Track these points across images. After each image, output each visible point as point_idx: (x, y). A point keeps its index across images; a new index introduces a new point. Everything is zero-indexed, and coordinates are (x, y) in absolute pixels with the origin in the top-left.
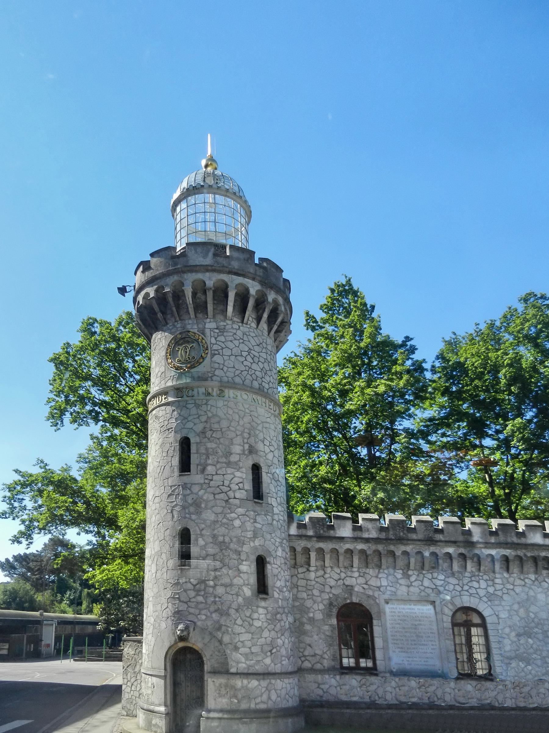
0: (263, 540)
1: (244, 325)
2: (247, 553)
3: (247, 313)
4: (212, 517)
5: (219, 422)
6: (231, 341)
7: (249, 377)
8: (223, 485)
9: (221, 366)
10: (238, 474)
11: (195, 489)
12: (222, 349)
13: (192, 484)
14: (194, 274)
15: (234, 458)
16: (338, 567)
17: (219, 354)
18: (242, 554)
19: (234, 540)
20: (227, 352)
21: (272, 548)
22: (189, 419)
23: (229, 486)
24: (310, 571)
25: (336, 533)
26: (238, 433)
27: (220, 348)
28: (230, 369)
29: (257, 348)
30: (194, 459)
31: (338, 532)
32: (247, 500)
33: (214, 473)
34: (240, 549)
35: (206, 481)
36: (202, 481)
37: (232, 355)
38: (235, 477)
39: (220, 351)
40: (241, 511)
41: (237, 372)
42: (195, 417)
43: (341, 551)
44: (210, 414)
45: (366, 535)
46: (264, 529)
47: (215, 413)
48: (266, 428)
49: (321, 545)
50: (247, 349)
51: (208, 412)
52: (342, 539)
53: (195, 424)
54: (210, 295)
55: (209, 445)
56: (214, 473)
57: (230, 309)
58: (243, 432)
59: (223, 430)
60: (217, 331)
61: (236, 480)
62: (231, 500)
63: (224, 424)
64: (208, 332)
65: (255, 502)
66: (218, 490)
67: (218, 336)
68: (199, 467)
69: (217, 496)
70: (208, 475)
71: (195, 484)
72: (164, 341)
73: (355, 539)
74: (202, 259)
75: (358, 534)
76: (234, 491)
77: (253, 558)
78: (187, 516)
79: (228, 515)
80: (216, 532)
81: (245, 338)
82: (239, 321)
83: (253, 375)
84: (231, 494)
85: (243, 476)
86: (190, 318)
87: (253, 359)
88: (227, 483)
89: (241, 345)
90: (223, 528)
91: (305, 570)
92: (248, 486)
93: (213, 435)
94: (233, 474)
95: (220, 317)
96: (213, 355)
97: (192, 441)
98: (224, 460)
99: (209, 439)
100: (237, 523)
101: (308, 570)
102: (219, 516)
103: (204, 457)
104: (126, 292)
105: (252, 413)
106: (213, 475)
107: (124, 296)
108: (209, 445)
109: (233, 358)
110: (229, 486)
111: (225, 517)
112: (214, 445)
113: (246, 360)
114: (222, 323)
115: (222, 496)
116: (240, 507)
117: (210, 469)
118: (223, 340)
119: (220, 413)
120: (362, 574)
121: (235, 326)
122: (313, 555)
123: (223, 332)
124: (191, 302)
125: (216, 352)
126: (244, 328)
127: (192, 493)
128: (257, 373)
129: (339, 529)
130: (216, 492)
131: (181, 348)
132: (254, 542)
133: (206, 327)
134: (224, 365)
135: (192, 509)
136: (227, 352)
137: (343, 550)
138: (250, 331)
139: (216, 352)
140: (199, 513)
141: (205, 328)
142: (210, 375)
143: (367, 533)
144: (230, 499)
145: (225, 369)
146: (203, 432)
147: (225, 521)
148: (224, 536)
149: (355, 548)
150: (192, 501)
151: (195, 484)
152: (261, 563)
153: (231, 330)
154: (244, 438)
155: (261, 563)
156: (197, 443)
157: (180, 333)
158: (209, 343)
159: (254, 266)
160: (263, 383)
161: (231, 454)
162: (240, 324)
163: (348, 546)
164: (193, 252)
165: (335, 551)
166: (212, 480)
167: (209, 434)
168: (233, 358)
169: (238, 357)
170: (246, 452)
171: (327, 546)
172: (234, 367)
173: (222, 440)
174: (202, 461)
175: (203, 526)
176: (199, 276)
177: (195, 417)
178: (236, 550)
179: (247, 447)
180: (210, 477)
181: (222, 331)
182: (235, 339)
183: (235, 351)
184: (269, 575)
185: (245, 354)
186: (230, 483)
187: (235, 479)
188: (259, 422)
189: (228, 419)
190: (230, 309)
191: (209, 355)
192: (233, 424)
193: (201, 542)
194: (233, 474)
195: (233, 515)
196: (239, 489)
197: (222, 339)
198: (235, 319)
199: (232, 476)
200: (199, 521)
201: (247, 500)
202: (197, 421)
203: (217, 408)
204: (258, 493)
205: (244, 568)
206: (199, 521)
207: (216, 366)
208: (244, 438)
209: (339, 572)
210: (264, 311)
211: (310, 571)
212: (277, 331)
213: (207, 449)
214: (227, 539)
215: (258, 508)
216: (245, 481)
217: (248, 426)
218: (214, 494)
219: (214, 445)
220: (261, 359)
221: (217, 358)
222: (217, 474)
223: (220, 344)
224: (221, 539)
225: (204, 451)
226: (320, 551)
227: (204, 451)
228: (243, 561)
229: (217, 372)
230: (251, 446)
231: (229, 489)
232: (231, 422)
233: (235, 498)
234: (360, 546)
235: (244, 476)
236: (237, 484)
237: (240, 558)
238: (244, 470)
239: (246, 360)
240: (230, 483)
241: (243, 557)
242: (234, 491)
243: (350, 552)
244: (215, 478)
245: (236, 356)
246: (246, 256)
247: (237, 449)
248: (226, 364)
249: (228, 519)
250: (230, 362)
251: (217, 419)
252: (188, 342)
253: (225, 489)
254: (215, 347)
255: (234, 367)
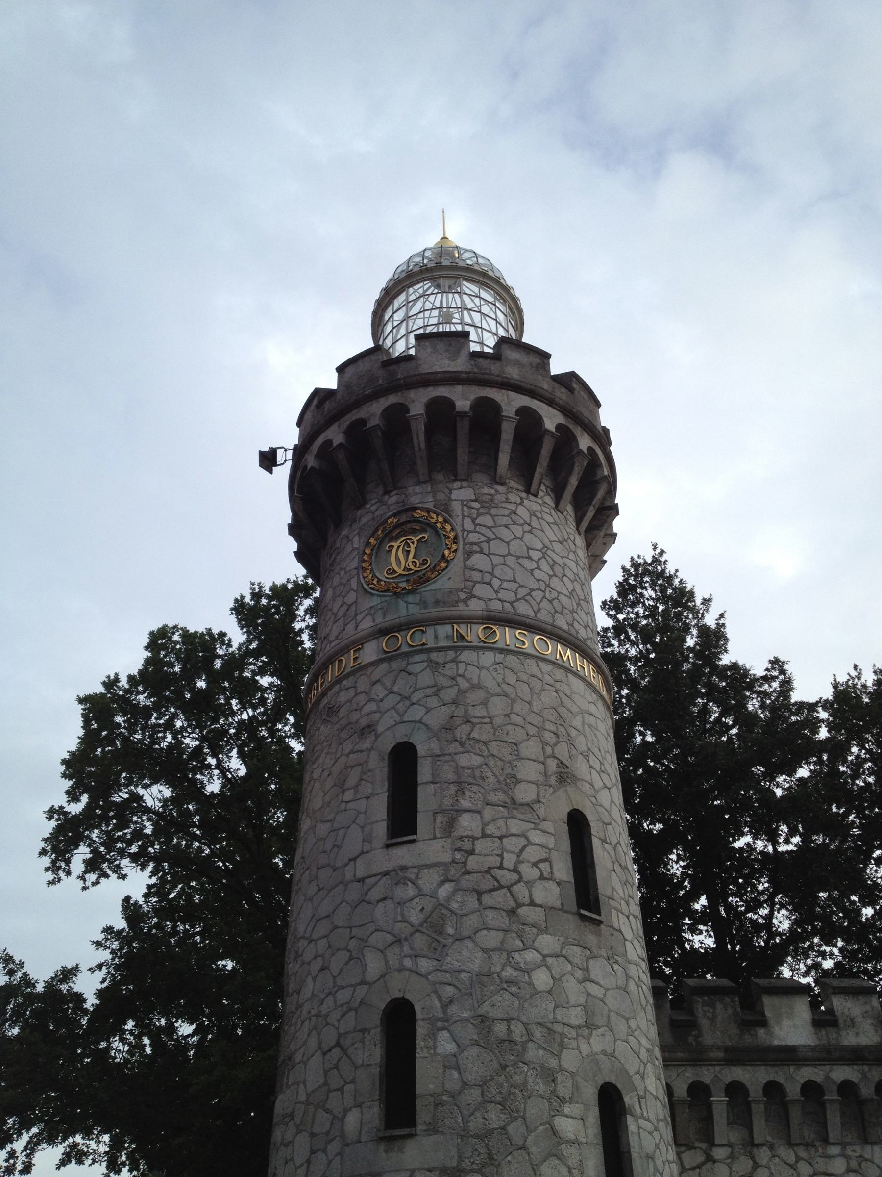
0: (609, 1037)
1: (532, 498)
2: (573, 1075)
3: (537, 476)
4: (477, 962)
5: (485, 703)
6: (506, 526)
7: (545, 604)
8: (501, 867)
9: (487, 578)
10: (536, 837)
11: (429, 879)
12: (489, 541)
13: (421, 867)
14: (430, 389)
15: (525, 793)
16: (790, 1144)
17: (481, 552)
18: (559, 1077)
19: (538, 1033)
20: (497, 547)
21: (632, 1066)
22: (414, 700)
23: (515, 870)
24: (715, 1162)
25: (770, 1034)
26: (532, 731)
27: (483, 539)
28: (506, 585)
29: (557, 547)
30: (427, 798)
31: (776, 1030)
32: (562, 909)
33: (478, 834)
34: (553, 1063)
35: (458, 856)
36: (446, 857)
37: (509, 554)
38: (530, 843)
39: (485, 546)
40: (547, 942)
41: (522, 592)
42: (429, 691)
43: (793, 1090)
44: (464, 684)
45: (849, 1039)
46: (609, 1000)
47: (476, 681)
48: (590, 726)
49: (738, 1073)
50: (539, 546)
51: (459, 679)
52: (788, 1055)
53: (429, 710)
54: (463, 429)
55: (464, 760)
56: (478, 834)
57: (504, 459)
58: (541, 729)
59: (498, 721)
60: (476, 505)
61: (533, 854)
62: (522, 911)
63: (498, 706)
64: (456, 507)
65: (583, 918)
66: (489, 883)
67: (479, 515)
68: (439, 818)
69: (487, 899)
70: (461, 838)
71: (428, 866)
72: (356, 539)
73: (828, 1055)
74: (447, 362)
75: (830, 1036)
76: (529, 884)
77: (590, 1093)
78: (408, 963)
79: (517, 956)
80: (485, 1008)
81: (535, 523)
82: (520, 488)
83: (555, 602)
84: (521, 890)
85: (551, 841)
86: (419, 483)
87: (552, 568)
88: (510, 860)
89: (528, 536)
90: (506, 996)
91: (701, 1158)
92: (563, 869)
93: (474, 735)
94: (523, 835)
95: (480, 478)
96: (469, 554)
97: (421, 751)
98: (499, 797)
99: (462, 744)
100: (541, 979)
101: (710, 1159)
102: (495, 957)
103: (453, 788)
104: (276, 465)
105: (558, 685)
106: (475, 838)
107: (271, 472)
108: (464, 760)
109: (511, 561)
110: (515, 870)
111: (509, 961)
112: (477, 760)
113: (538, 568)
114: (486, 490)
115: (499, 898)
116: (546, 931)
117: (467, 824)
118: (490, 523)
119: (489, 682)
120: (854, 1164)
121: (513, 497)
122: (719, 1099)
123: (489, 508)
124: (423, 446)
125: (476, 548)
126: (532, 504)
127: (421, 894)
128: (563, 599)
129: (779, 1022)
130: (484, 887)
131: (396, 545)
132: (588, 1039)
133: (453, 497)
134: (492, 574)
135: (420, 941)
136: (497, 547)
137: (798, 1089)
138: (542, 511)
139: (476, 548)
140: (438, 950)
141: (450, 499)
142: (463, 596)
143: (851, 1032)
144: (519, 905)
145: (496, 583)
146: (448, 728)
147: (509, 973)
148: (509, 1020)
149: (827, 1078)
150: (422, 916)
151: (428, 866)
152: (611, 1104)
153: (506, 505)
154: (545, 744)
155: (611, 1104)
156: (435, 756)
157: (394, 515)
158: (459, 529)
159: (549, 379)
160: (576, 624)
161: (519, 782)
162: (524, 495)
163: (807, 1073)
164: (429, 350)
165: (773, 1089)
166: (472, 852)
167: (462, 731)
168: (511, 561)
169: (521, 560)
170: (553, 780)
171: (754, 1077)
172: (514, 581)
173: (494, 747)
174: (448, 802)
175: (450, 990)
176: (443, 391)
177: (429, 691)
178: (542, 1066)
179: (552, 765)
180: (467, 845)
181: (488, 505)
182: (515, 523)
183: (515, 546)
184: (635, 1155)
185: (535, 555)
186: (519, 862)
187: (528, 849)
188: (574, 709)
189: (507, 696)
190: (504, 459)
191: (460, 554)
192: (517, 707)
193: (446, 1045)
194: (523, 835)
195: (531, 956)
196: (542, 878)
197: (487, 520)
198: (513, 484)
199: (523, 842)
200: (440, 977)
201: (562, 909)
202: (433, 702)
203: (480, 668)
204: (586, 896)
205: (567, 1126)
206: (440, 977)
207: (476, 576)
208: (545, 744)
209: (792, 1159)
210: (570, 473)
211: (715, 1162)
212: (589, 530)
213: (457, 769)
214: (518, 1031)
215: (591, 939)
216: (554, 854)
217: (550, 715)
218: (480, 893)
219: (477, 760)
220: (568, 572)
221: (477, 560)
222: (484, 835)
223: (484, 530)
224: (500, 1029)
225: (451, 776)
226: (735, 1090)
227: (451, 776)
228: (562, 1101)
229: (479, 590)
230: (561, 764)
231: (515, 877)
232: (513, 701)
233: (532, 904)
234: (842, 1073)
235: (551, 842)
236: (535, 864)
237: (554, 1092)
238: (548, 826)
239: (538, 568)
240: (519, 862)
241: (564, 1088)
242: (529, 884)
243: (811, 1089)
244: (481, 846)
245: (518, 557)
246: (536, 360)
247: (529, 771)
248: (497, 572)
249: (517, 968)
250: (506, 569)
251: (479, 695)
252: (414, 532)
253: (506, 877)
254: (473, 537)
255: (514, 581)
